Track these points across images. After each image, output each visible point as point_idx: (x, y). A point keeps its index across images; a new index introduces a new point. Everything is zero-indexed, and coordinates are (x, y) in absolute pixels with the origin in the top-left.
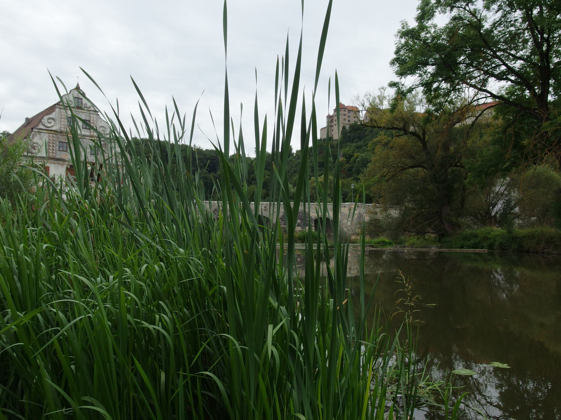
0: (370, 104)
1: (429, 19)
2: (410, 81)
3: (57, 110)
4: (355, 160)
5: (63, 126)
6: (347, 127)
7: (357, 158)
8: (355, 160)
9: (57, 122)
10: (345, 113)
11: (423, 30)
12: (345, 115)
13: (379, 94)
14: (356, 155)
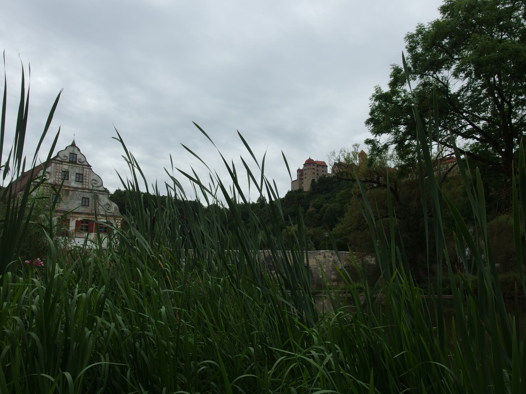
0: (345, 159)
1: (401, 85)
2: (384, 138)
3: (53, 164)
4: (324, 210)
5: (57, 179)
6: (316, 180)
7: (326, 208)
8: (324, 210)
9: (52, 176)
10: (314, 167)
11: (395, 95)
12: (314, 169)
13: (353, 150)
14: (325, 205)
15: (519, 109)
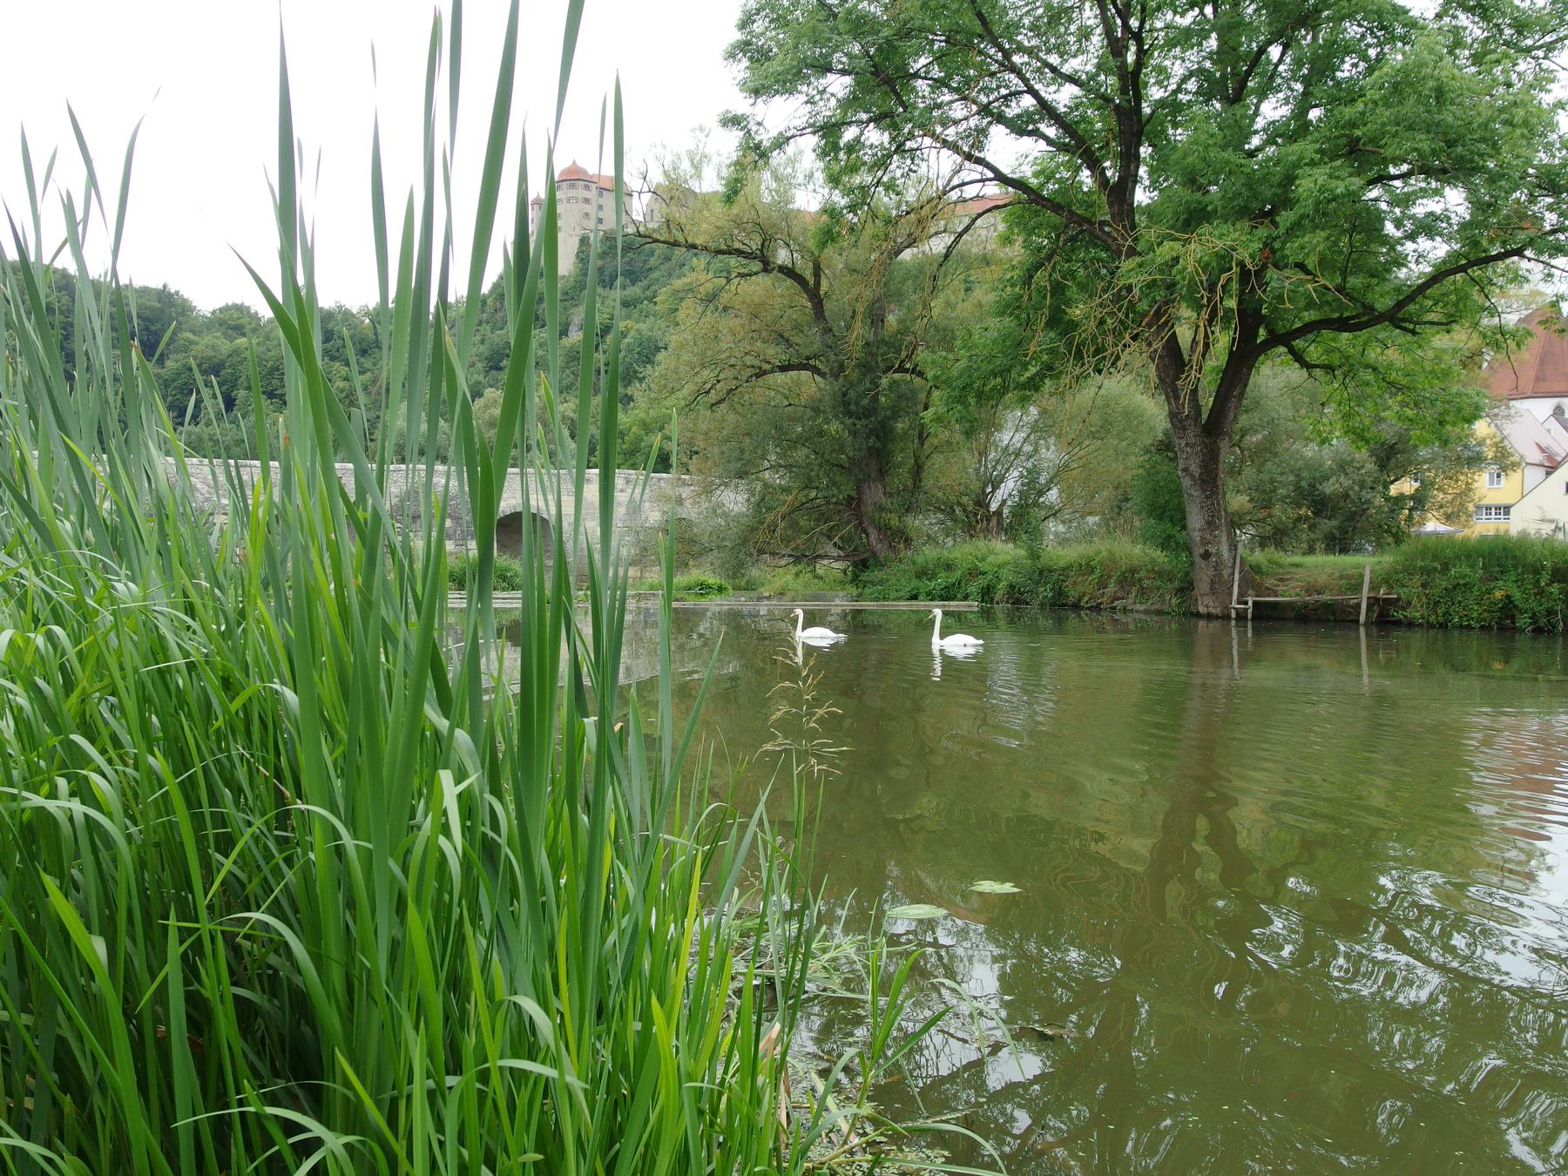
2: (782, 113)
12: (587, 201)
13: (692, 147)
15: (1175, 57)
